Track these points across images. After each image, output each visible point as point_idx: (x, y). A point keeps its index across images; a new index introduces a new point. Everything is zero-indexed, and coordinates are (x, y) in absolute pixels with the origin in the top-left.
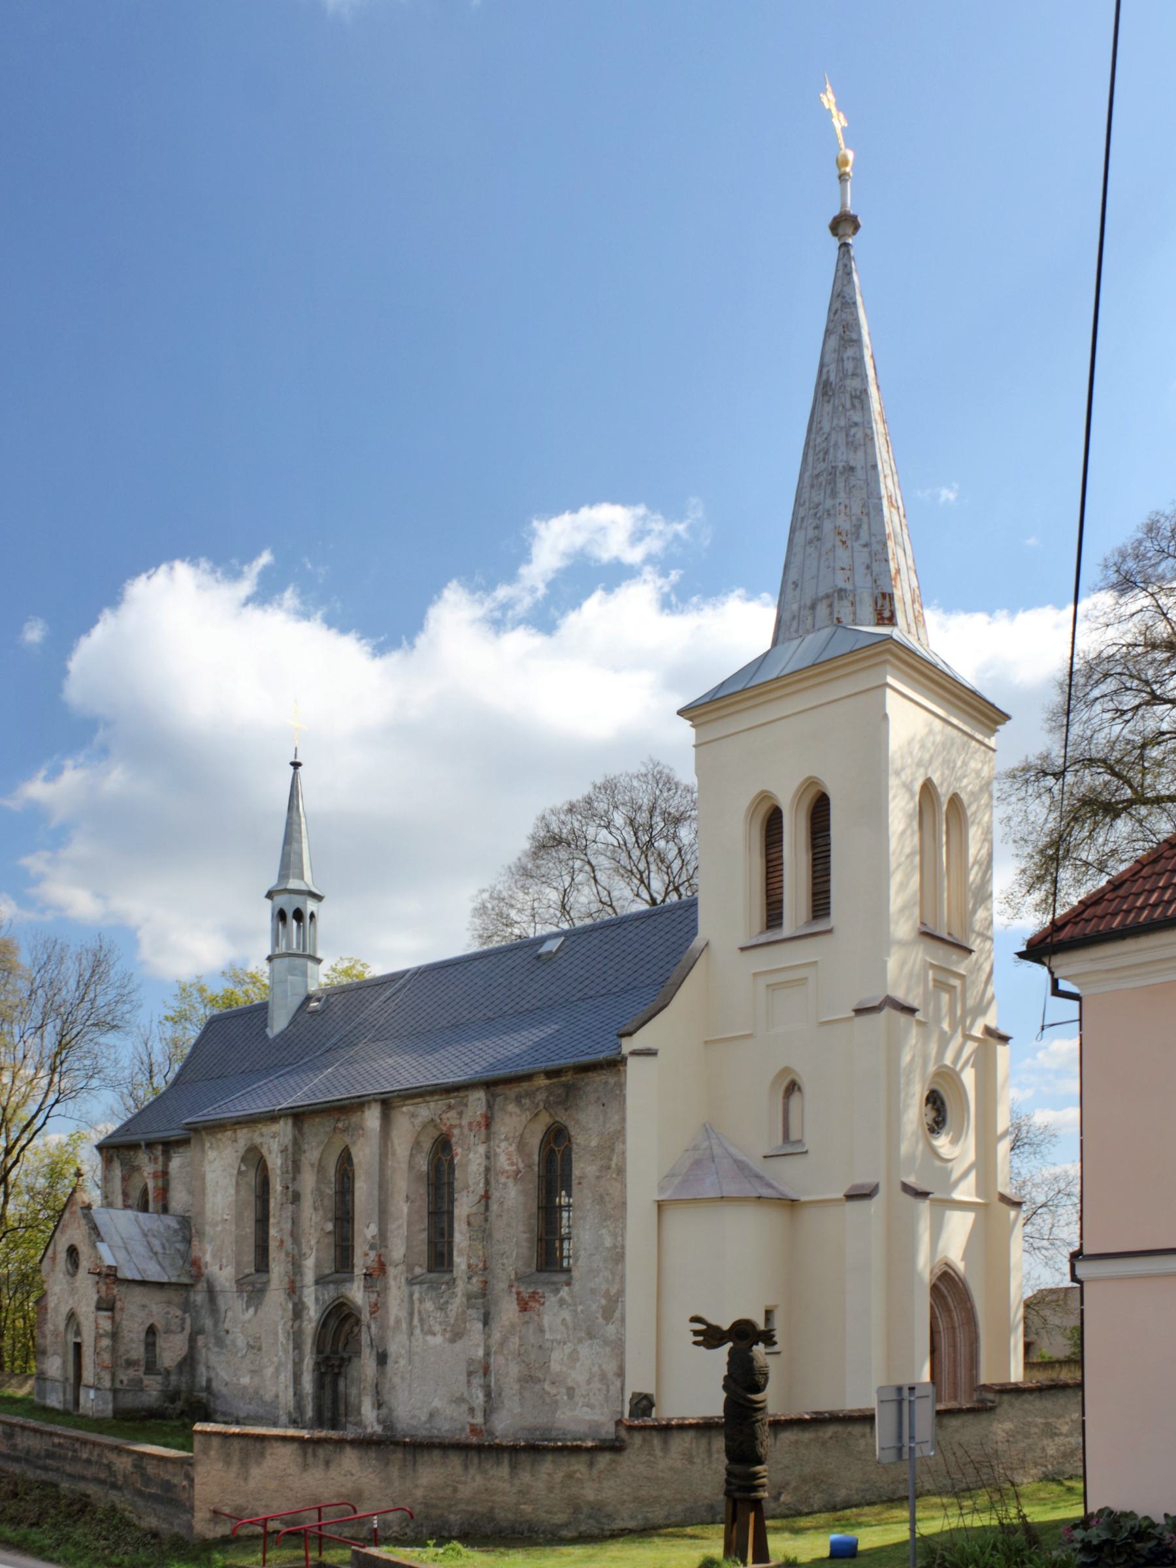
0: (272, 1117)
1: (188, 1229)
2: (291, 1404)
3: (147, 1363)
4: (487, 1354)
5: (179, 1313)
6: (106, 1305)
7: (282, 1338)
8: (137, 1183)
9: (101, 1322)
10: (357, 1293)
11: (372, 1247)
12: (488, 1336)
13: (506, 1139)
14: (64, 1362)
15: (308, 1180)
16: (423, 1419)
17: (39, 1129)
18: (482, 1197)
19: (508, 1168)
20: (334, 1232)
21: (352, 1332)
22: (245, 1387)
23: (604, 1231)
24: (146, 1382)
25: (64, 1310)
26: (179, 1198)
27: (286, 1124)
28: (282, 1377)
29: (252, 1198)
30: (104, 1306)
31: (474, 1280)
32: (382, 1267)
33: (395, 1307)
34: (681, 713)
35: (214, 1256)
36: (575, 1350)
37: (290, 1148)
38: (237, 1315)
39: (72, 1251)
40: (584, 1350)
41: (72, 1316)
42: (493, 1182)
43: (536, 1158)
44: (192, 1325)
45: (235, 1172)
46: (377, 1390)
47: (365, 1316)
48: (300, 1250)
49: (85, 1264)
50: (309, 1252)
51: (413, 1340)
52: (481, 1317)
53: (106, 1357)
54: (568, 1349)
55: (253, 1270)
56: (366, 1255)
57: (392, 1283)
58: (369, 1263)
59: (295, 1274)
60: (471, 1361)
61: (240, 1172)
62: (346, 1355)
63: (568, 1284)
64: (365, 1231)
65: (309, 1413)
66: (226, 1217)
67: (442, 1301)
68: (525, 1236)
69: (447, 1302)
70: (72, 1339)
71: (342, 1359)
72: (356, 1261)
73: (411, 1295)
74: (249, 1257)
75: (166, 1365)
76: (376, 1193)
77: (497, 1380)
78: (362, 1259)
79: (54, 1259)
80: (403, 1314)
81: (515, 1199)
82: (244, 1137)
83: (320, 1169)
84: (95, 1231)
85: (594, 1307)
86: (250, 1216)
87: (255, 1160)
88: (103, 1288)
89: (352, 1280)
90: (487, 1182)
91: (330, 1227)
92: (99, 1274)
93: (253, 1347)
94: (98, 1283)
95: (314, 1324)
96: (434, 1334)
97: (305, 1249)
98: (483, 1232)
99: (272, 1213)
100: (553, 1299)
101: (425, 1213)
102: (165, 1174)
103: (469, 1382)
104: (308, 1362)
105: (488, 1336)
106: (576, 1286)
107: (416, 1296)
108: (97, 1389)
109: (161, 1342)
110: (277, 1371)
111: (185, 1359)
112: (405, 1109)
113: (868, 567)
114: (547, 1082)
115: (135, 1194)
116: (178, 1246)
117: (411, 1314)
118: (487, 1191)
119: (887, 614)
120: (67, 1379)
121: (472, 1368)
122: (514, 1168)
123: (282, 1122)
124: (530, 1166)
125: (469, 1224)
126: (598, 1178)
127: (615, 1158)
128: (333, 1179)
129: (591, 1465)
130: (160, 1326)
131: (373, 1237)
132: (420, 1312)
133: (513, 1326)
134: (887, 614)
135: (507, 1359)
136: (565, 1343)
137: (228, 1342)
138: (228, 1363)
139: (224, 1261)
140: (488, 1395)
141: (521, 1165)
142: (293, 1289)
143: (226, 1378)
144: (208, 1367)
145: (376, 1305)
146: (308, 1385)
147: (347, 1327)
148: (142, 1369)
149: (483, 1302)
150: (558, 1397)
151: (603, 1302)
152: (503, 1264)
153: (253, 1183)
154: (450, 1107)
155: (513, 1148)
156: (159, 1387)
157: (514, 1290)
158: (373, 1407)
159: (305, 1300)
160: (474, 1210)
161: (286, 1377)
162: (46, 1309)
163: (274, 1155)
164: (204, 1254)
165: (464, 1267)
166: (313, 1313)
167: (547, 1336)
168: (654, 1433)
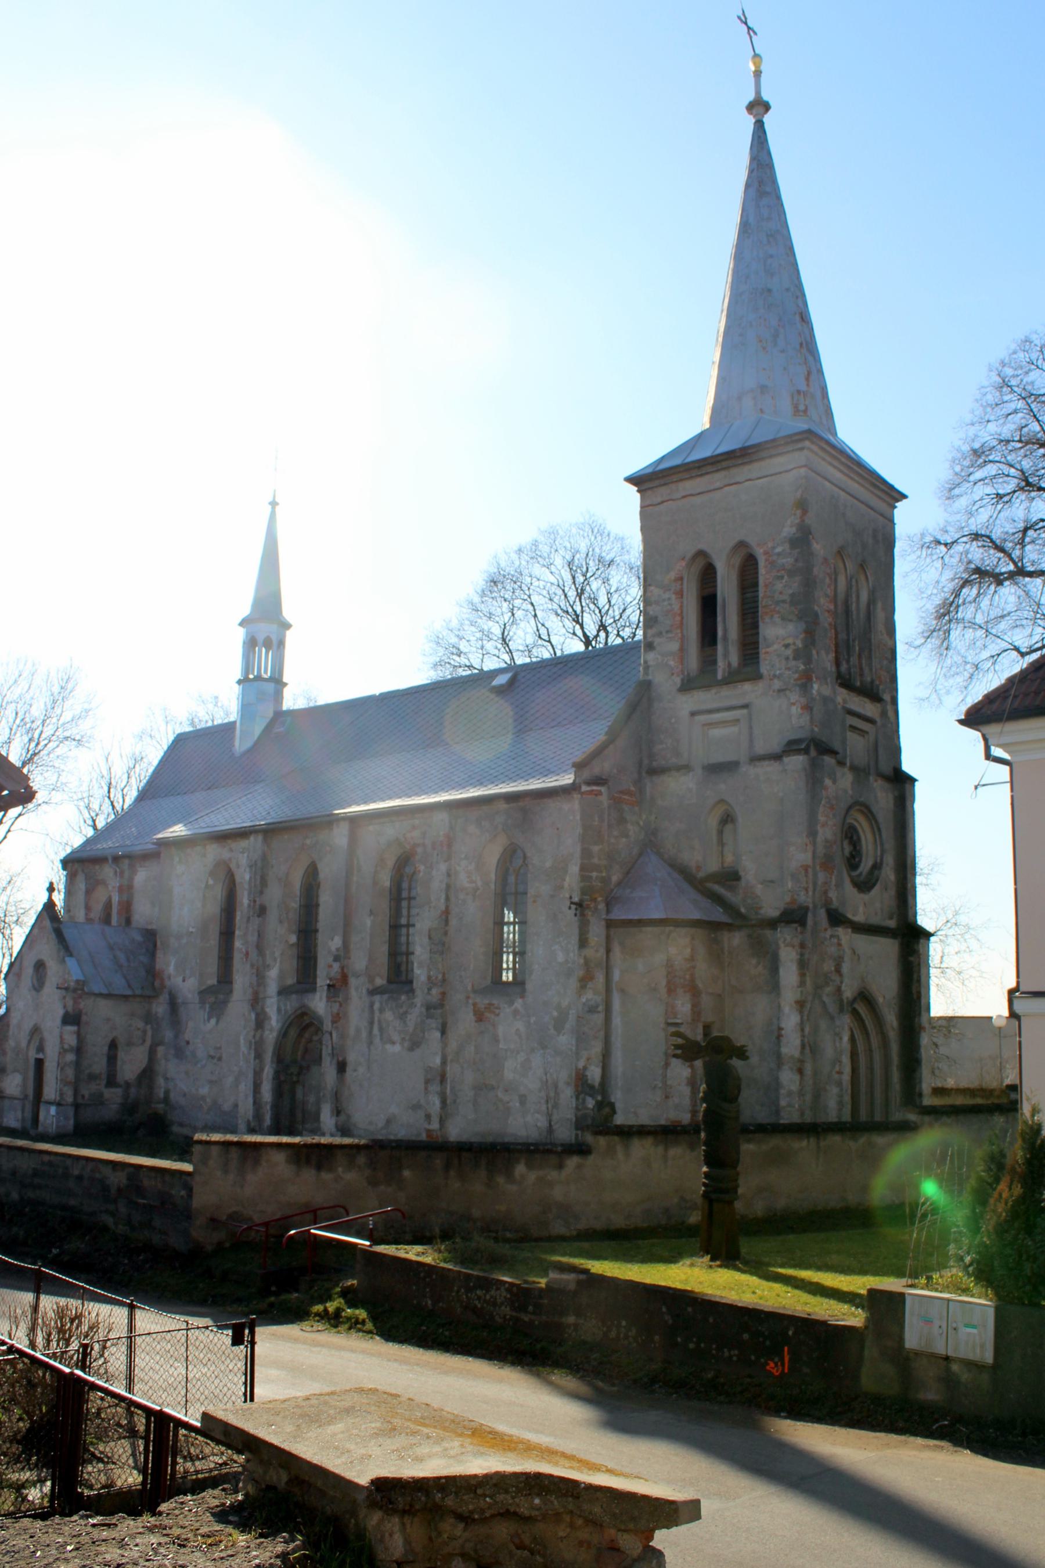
2: (250, 1114)
4: (444, 1062)
5: (141, 1024)
7: (244, 1048)
8: (100, 896)
9: (66, 1037)
10: (319, 1004)
11: (337, 959)
12: (445, 1044)
14: (25, 1080)
16: (380, 1125)
19: (468, 885)
20: (298, 944)
23: (557, 947)
25: (27, 1026)
28: (242, 1087)
31: (434, 991)
32: (344, 978)
34: (633, 480)
38: (200, 1028)
41: (36, 1030)
43: (493, 876)
44: (152, 1036)
46: (337, 1097)
47: (327, 1025)
52: (440, 1026)
53: (70, 1073)
54: (521, 1057)
56: (330, 966)
57: (353, 993)
58: (332, 974)
59: (259, 985)
61: (207, 886)
63: (522, 997)
64: (329, 943)
65: (268, 1121)
66: (191, 930)
67: (401, 1011)
69: (406, 1013)
70: (33, 1055)
71: (301, 1068)
72: (318, 973)
73: (372, 1005)
75: (127, 1078)
77: (452, 1088)
89: (313, 990)
90: (447, 899)
91: (293, 939)
92: (66, 989)
94: (64, 998)
95: (275, 1034)
96: (394, 1043)
97: (269, 961)
100: (508, 1010)
103: (426, 1089)
104: (268, 1072)
105: (445, 1044)
107: (377, 1006)
108: (59, 1104)
109: (121, 1055)
110: (237, 1082)
111: (144, 1071)
112: (371, 828)
113: (785, 369)
114: (505, 806)
115: (98, 909)
116: (142, 958)
118: (447, 907)
119: (802, 407)
120: (26, 1097)
123: (252, 838)
125: (430, 938)
126: (552, 896)
127: (568, 879)
128: (298, 893)
131: (338, 950)
132: (379, 1021)
134: (802, 407)
136: (518, 1053)
137: (188, 1053)
139: (187, 972)
140: (444, 1102)
141: (479, 883)
142: (256, 1001)
144: (167, 1079)
145: (338, 1014)
146: (267, 1094)
147: (307, 1035)
148: (104, 1082)
150: (511, 1104)
151: (555, 1014)
152: (461, 977)
153: (219, 897)
156: (119, 1100)
158: (332, 1112)
159: (267, 1010)
161: (245, 1087)
162: (8, 1026)
165: (423, 978)
166: (274, 1022)
167: (501, 1046)
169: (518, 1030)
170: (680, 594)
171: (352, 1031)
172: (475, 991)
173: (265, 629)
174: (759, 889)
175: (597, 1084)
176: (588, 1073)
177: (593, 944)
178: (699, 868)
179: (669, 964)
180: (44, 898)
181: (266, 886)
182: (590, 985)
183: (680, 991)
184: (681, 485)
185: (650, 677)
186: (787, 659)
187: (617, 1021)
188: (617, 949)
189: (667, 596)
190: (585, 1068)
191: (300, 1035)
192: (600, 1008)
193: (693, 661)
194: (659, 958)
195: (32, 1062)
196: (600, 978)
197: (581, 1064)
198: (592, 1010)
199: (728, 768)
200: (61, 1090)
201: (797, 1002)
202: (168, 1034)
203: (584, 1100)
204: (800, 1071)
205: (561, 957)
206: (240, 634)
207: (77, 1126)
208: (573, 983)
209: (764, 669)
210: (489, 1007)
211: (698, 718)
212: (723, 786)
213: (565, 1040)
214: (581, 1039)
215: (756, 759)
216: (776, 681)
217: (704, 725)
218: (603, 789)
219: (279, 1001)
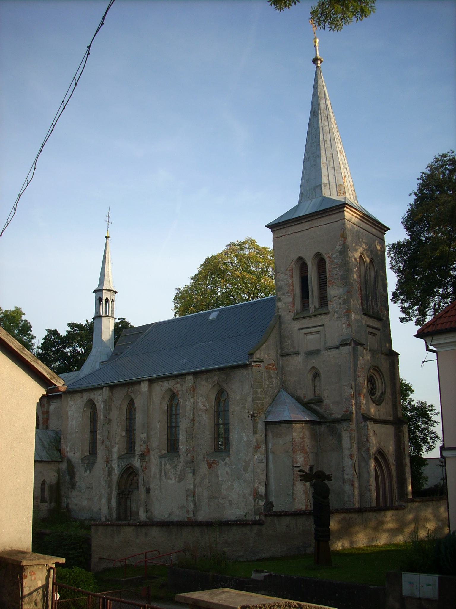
4: (195, 487)
7: (103, 483)
10: (137, 463)
11: (144, 442)
13: (201, 396)
21: (133, 479)
23: (243, 434)
24: (41, 507)
31: (189, 455)
32: (148, 451)
33: (154, 469)
35: (71, 449)
42: (196, 413)
45: (82, 411)
60: (188, 490)
61: (84, 411)
62: (130, 490)
64: (140, 436)
68: (210, 436)
69: (177, 465)
73: (161, 463)
74: (87, 448)
78: (138, 452)
81: (206, 421)
82: (86, 396)
86: (87, 430)
87: (91, 405)
90: (194, 414)
91: (124, 434)
93: (88, 488)
95: (117, 477)
98: (191, 435)
107: (163, 463)
118: (194, 418)
121: (188, 493)
123: (104, 389)
125: (186, 432)
132: (164, 470)
135: (203, 489)
141: (208, 407)
142: (108, 461)
143: (75, 502)
147: (131, 477)
149: (192, 465)
151: (244, 464)
154: (177, 383)
157: (205, 459)
166: (117, 472)
168: (275, 518)
170: (291, 276)
172: (207, 455)
175: (263, 494)
178: (305, 397)
184: (290, 228)
185: (280, 313)
187: (271, 466)
188: (270, 434)
189: (286, 277)
190: (258, 487)
192: (264, 461)
193: (298, 306)
196: (263, 447)
199: (317, 352)
203: (258, 502)
205: (245, 439)
207: (23, 566)
211: (302, 331)
212: (314, 361)
215: (328, 349)
218: (261, 364)
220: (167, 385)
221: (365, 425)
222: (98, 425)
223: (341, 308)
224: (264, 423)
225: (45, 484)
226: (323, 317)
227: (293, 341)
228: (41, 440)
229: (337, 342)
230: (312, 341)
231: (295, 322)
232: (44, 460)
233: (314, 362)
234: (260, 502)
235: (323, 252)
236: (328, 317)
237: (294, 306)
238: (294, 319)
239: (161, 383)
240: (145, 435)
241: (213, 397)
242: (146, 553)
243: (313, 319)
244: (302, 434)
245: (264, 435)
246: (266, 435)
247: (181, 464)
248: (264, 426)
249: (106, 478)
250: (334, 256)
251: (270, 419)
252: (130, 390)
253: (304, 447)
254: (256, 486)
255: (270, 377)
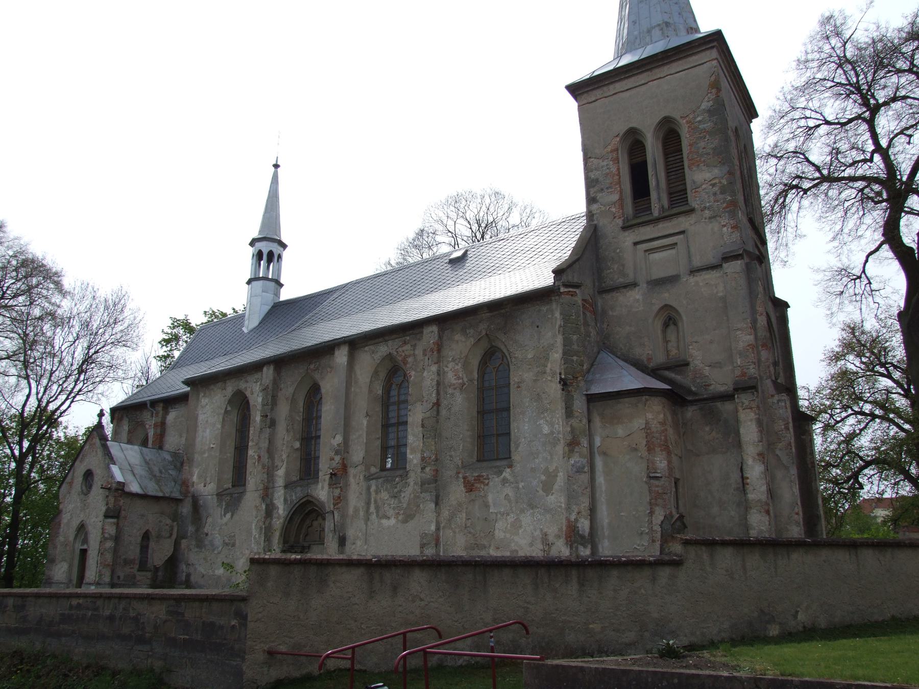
0: (256, 367)
1: (180, 461)
3: (140, 562)
4: (438, 529)
5: (169, 521)
6: (112, 514)
7: (255, 532)
10: (322, 492)
11: (337, 452)
12: (438, 514)
13: (453, 360)
15: (283, 410)
17: (65, 411)
18: (434, 404)
21: (312, 525)
22: (219, 577)
23: (542, 422)
24: (138, 578)
25: (75, 523)
26: (173, 440)
27: (268, 369)
29: (234, 431)
30: (111, 514)
31: (427, 469)
32: (344, 467)
33: (354, 500)
35: (200, 477)
36: (518, 520)
37: (270, 387)
38: (217, 522)
39: (89, 475)
40: (526, 519)
41: (82, 528)
42: (442, 393)
45: (223, 411)
48: (273, 464)
49: (98, 481)
50: (280, 464)
51: (369, 523)
52: (434, 498)
53: (109, 557)
54: (511, 518)
55: (230, 486)
57: (352, 480)
59: (268, 482)
60: (424, 536)
61: (226, 412)
62: (306, 544)
63: (510, 466)
64: (330, 440)
67: (396, 490)
68: (469, 433)
69: (400, 491)
70: (79, 546)
73: (369, 488)
74: (228, 475)
75: (156, 564)
76: (342, 411)
78: (325, 467)
79: (71, 484)
80: (361, 504)
81: (460, 405)
82: (230, 388)
83: (293, 401)
84: (109, 457)
85: (535, 483)
86: (231, 445)
87: (241, 403)
88: (112, 500)
90: (438, 394)
91: (297, 445)
92: (109, 489)
93: (227, 544)
95: (282, 520)
98: (433, 429)
99: (251, 438)
101: (379, 426)
102: (163, 424)
105: (438, 514)
106: (518, 468)
107: (373, 488)
109: (152, 544)
117: (368, 504)
118: (438, 400)
121: (425, 541)
122: (460, 381)
123: (265, 369)
124: (471, 380)
125: (423, 426)
126: (535, 381)
127: (549, 365)
128: (302, 410)
129: (654, 580)
130: (153, 533)
132: (376, 501)
133: (460, 505)
135: (454, 532)
136: (508, 514)
138: (205, 559)
139: (208, 479)
141: (465, 380)
142: (267, 493)
143: (202, 571)
145: (339, 498)
147: (308, 522)
149: (435, 487)
151: (543, 478)
152: (451, 456)
154: (405, 343)
155: (459, 367)
157: (461, 476)
159: (275, 502)
160: (428, 414)
163: (255, 395)
164: (192, 476)
166: (281, 510)
168: (704, 548)
169: (507, 495)
170: (616, 160)
171: (351, 511)
172: (464, 467)
173: (268, 250)
174: (707, 371)
175: (586, 534)
176: (579, 525)
177: (576, 414)
178: (649, 359)
179: (647, 428)
180: (95, 420)
181: (276, 405)
182: (577, 449)
183: (658, 449)
184: (611, 87)
185: (595, 222)
186: (715, 194)
187: (600, 479)
188: (597, 421)
189: (605, 163)
190: (576, 520)
191: (303, 520)
192: (586, 469)
193: (629, 208)
194: (638, 423)
195: (78, 552)
196: (585, 442)
197: (573, 517)
198: (579, 471)
199: (672, 280)
200: (100, 571)
201: (759, 455)
202: (191, 529)
203: (577, 548)
204: (768, 512)
206: (250, 251)
208: (560, 448)
209: (694, 203)
210: (479, 479)
211: (639, 246)
212: (666, 295)
213: (556, 499)
214: (571, 498)
215: (694, 271)
216: (707, 212)
217: (646, 251)
218: (578, 291)
219: (285, 493)
220: (383, 350)
221: (779, 401)
222: (251, 432)
223: (718, 201)
224: (584, 398)
225: (148, 539)
226: (682, 219)
227: (623, 265)
228: (147, 463)
229: (711, 257)
230: (662, 263)
231: (626, 234)
232: (150, 493)
233: (667, 296)
234: (581, 548)
235: (676, 115)
236: (692, 218)
237: (622, 207)
238: (625, 228)
239: (372, 347)
240: (339, 439)
241: (475, 362)
242: (404, 634)
243: (661, 225)
244: (662, 416)
245: (585, 421)
246: (589, 421)
247: (410, 489)
248: (585, 403)
249: (261, 524)
250: (699, 119)
251: (596, 389)
252: (312, 366)
253: (666, 441)
254: (573, 517)
255: (586, 324)
